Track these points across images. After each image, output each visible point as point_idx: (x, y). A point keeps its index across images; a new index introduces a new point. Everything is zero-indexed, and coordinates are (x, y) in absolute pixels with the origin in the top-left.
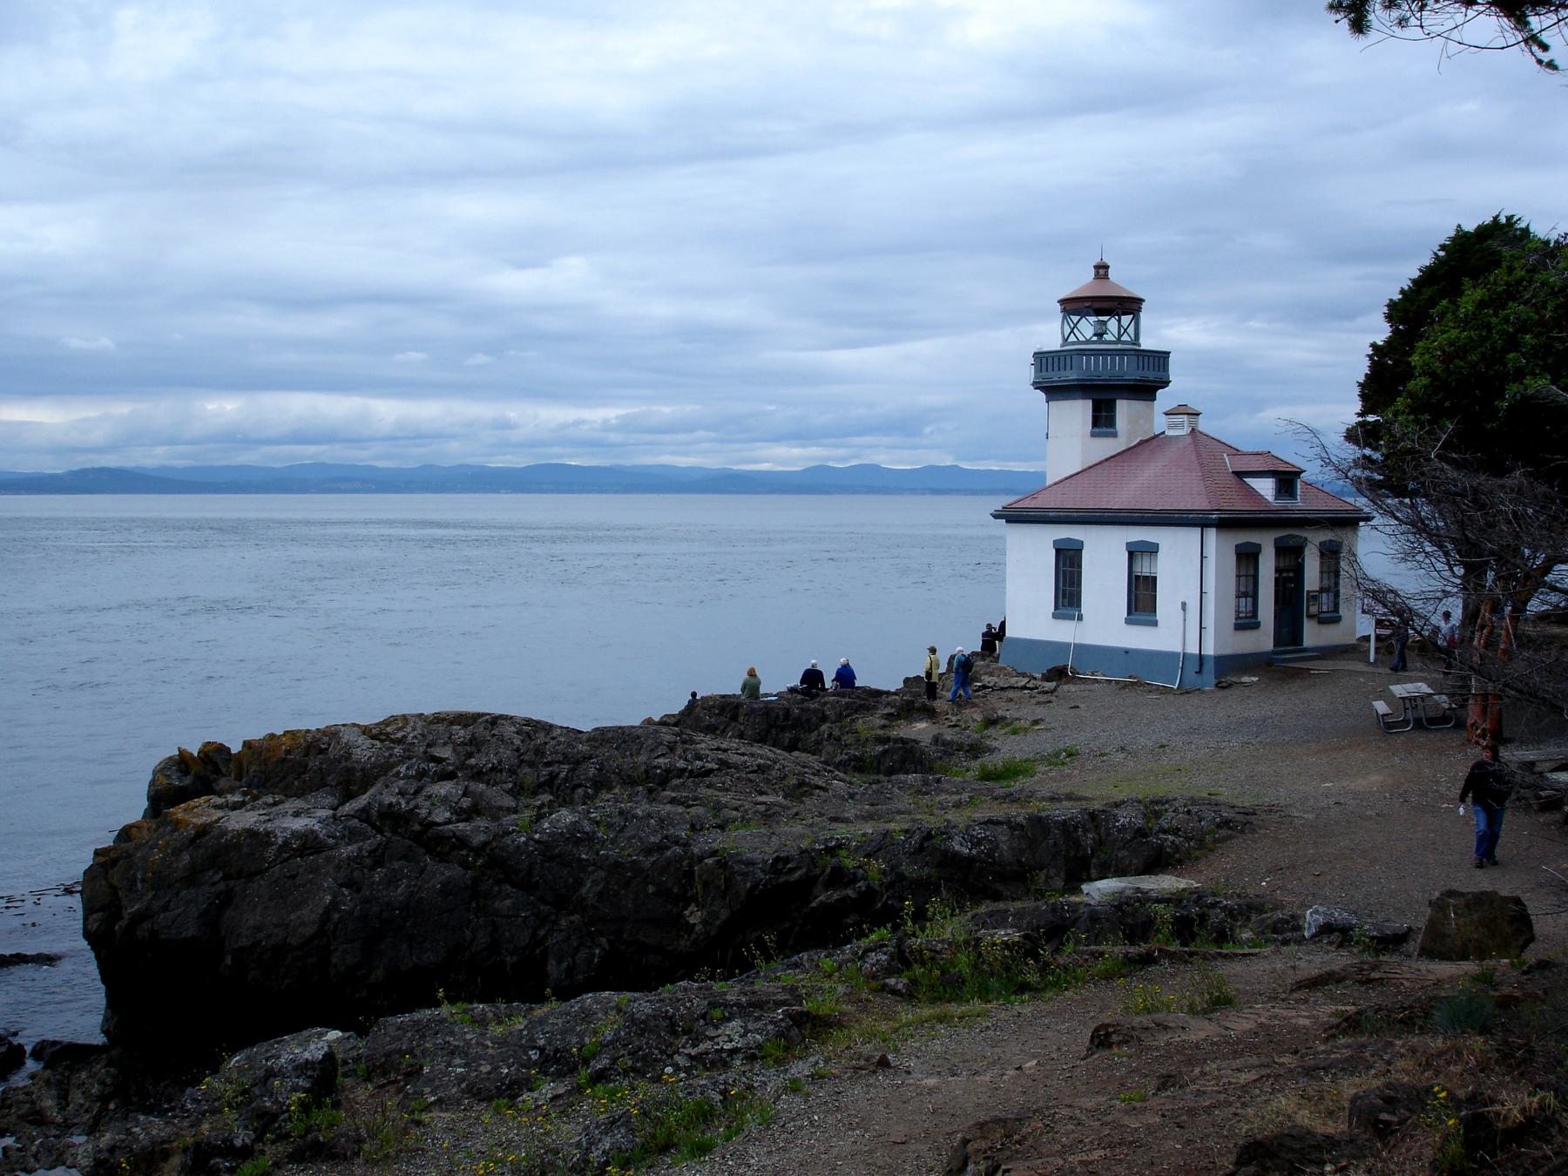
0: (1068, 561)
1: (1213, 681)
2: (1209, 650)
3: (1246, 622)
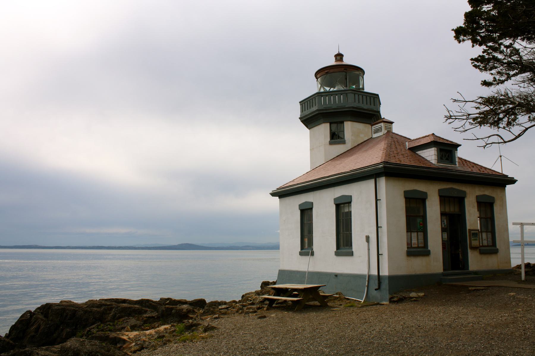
0: (306, 212)
1: (388, 296)
2: (385, 272)
3: (417, 251)
